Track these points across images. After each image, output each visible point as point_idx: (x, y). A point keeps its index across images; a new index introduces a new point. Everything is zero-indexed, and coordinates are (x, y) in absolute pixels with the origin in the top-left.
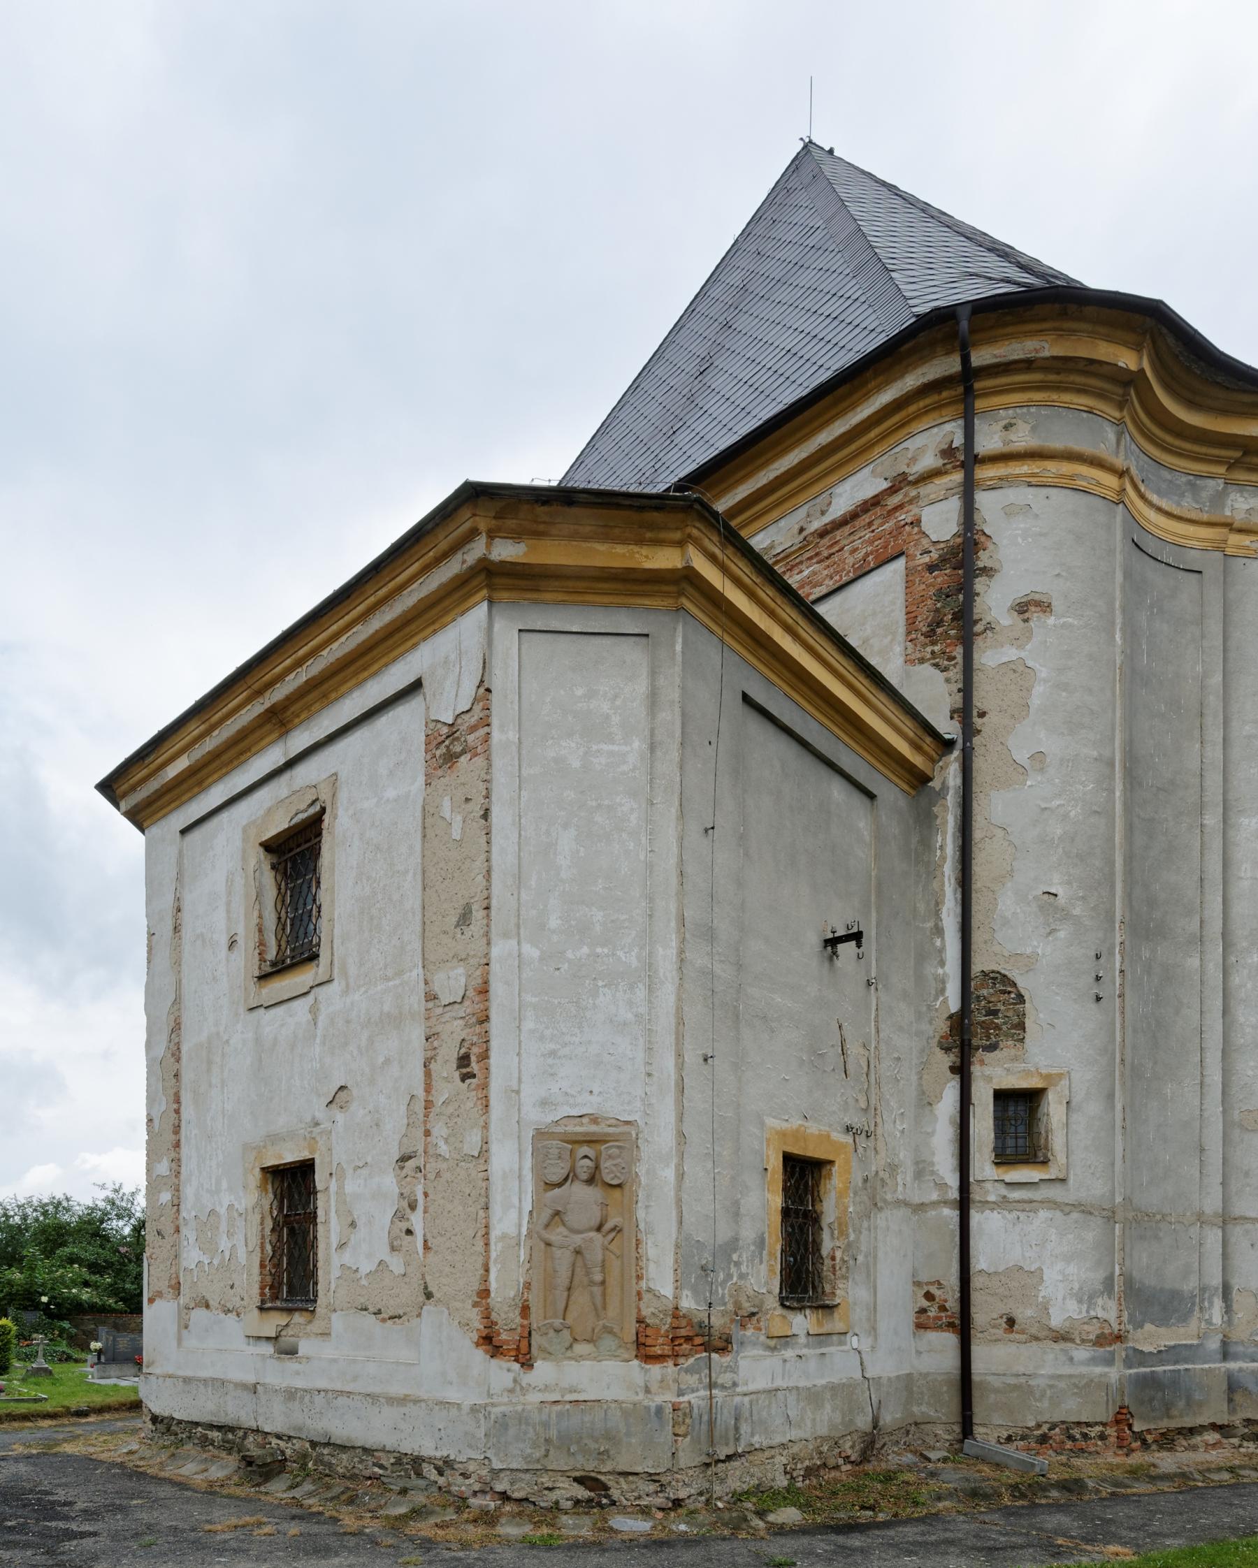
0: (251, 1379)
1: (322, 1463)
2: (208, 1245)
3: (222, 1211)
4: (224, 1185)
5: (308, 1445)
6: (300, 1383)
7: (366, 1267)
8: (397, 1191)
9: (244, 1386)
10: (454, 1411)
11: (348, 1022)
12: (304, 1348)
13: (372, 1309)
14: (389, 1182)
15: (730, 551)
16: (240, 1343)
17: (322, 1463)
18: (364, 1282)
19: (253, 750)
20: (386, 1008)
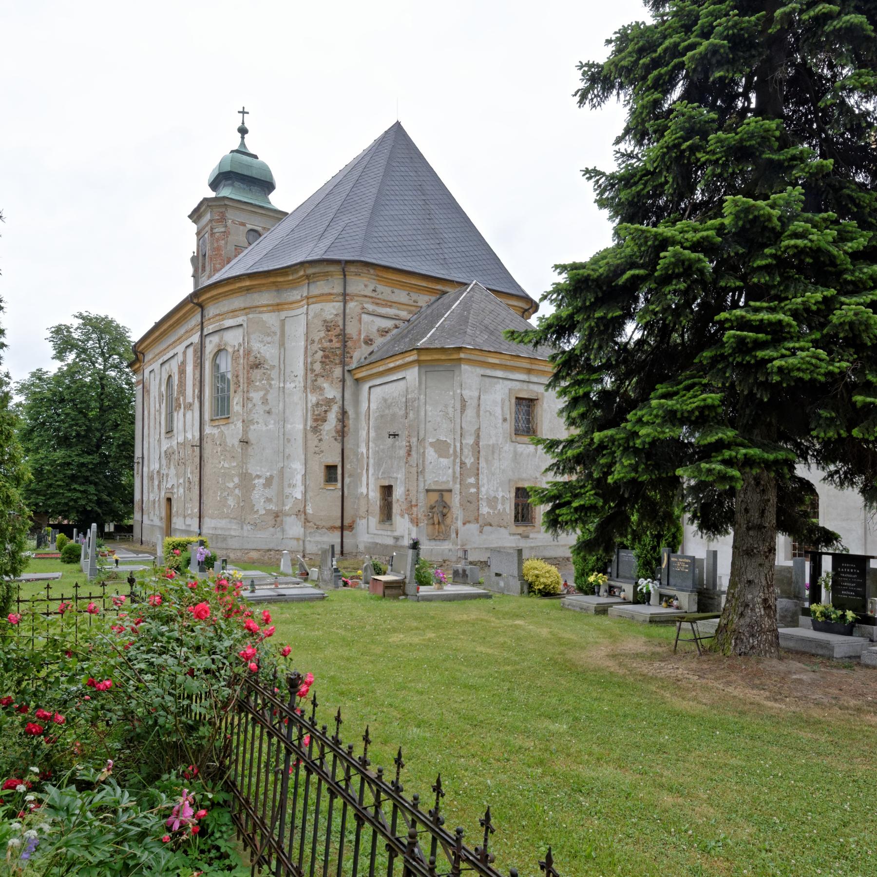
3: (500, 497)
4: (500, 489)
6: (532, 545)
12: (531, 536)
15: (450, 354)
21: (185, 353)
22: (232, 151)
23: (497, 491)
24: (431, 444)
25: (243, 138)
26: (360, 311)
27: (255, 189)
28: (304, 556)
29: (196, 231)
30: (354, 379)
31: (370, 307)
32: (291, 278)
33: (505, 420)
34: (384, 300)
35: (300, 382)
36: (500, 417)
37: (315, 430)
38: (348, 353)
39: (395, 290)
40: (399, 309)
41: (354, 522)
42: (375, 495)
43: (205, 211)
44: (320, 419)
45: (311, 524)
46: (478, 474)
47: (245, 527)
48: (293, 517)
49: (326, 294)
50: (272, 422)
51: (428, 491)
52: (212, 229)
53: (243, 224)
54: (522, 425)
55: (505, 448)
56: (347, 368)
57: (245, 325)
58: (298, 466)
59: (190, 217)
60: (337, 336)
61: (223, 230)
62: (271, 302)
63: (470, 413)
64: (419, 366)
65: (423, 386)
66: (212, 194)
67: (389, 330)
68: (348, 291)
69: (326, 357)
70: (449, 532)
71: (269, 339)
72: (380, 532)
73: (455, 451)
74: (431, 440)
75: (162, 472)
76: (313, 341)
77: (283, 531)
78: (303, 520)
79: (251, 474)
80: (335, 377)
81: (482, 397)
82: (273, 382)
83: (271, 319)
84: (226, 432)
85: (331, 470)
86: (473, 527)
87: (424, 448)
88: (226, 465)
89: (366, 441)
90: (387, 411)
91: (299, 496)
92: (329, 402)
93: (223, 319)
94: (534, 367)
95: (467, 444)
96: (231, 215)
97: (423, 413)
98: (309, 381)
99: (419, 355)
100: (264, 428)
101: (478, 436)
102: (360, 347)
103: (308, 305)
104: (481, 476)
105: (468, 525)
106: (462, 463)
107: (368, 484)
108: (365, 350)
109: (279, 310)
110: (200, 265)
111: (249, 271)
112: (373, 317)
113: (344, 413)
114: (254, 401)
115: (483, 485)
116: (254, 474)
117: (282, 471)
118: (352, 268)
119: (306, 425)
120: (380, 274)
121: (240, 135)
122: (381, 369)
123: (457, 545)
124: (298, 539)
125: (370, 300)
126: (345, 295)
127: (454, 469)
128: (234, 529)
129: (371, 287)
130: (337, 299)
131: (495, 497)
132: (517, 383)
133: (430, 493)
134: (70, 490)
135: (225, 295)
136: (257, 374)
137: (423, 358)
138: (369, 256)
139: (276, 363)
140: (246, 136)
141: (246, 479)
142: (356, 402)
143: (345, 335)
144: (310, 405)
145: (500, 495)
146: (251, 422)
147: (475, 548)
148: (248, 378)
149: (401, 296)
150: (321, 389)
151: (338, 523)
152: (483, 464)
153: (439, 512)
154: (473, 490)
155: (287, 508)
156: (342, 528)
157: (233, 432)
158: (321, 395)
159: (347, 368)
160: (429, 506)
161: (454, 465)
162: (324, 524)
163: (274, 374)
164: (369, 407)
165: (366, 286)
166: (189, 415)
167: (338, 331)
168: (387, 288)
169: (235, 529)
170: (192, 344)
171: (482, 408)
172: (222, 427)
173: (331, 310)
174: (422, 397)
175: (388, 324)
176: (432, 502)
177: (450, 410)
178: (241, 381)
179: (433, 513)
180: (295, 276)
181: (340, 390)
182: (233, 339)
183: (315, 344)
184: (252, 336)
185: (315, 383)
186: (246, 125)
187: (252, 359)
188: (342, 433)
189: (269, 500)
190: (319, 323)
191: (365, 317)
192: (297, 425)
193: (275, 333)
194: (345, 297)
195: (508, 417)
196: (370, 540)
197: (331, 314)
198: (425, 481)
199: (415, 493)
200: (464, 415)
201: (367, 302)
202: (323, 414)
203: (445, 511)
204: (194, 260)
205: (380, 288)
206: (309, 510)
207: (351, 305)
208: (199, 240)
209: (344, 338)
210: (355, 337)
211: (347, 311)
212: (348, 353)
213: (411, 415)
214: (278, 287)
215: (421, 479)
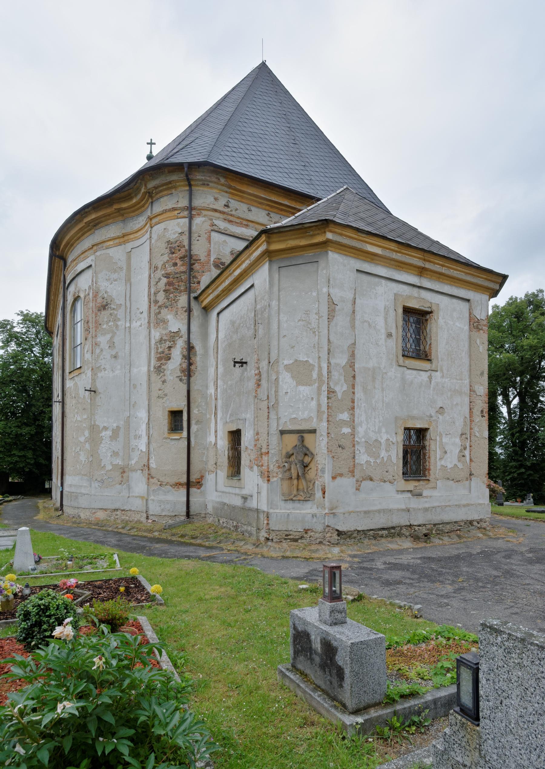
0: (403, 507)
1: (439, 530)
3: (383, 441)
4: (384, 430)
5: (432, 526)
6: (427, 505)
7: (450, 466)
8: (460, 444)
9: (403, 510)
10: (483, 506)
11: (443, 387)
12: (425, 493)
13: (451, 479)
14: (458, 440)
17: (439, 530)
18: (449, 470)
19: (404, 269)
20: (457, 388)
23: (380, 432)
24: (287, 368)
26: (210, 228)
28: (147, 518)
31: (222, 225)
32: (134, 201)
33: (389, 335)
34: (239, 218)
36: (383, 331)
37: (159, 370)
38: (194, 277)
39: (253, 208)
41: (202, 477)
42: (223, 443)
44: (165, 357)
45: (154, 481)
46: (353, 408)
47: (93, 485)
48: (139, 472)
50: (119, 367)
51: (282, 432)
54: (411, 345)
55: (389, 374)
58: (143, 414)
63: (341, 321)
64: (270, 261)
65: (276, 289)
69: (169, 284)
71: (115, 276)
73: (320, 374)
74: (286, 362)
76: (156, 268)
77: (129, 488)
78: (147, 475)
79: (98, 426)
80: (180, 306)
81: (358, 301)
82: (119, 323)
83: (117, 253)
85: (175, 415)
86: (347, 482)
87: (278, 373)
88: (79, 419)
90: (235, 337)
92: (174, 336)
94: (428, 265)
95: (337, 365)
98: (152, 315)
101: (353, 355)
103: (152, 227)
104: (357, 411)
105: (339, 479)
106: (331, 392)
107: (216, 432)
109: (125, 242)
112: (220, 229)
113: (190, 348)
114: (102, 346)
115: (360, 424)
117: (128, 421)
118: (198, 176)
119: (149, 366)
120: (233, 184)
122: (227, 282)
123: (324, 507)
124: (142, 498)
125: (221, 216)
126: (190, 208)
127: (318, 400)
130: (182, 214)
131: (376, 440)
133: (286, 436)
134: (10, 456)
136: (105, 314)
142: (205, 336)
143: (191, 257)
144: (153, 342)
145: (384, 437)
147: (350, 513)
150: (165, 322)
152: (359, 394)
153: (298, 464)
154: (346, 430)
155: (133, 462)
156: (188, 485)
158: (165, 329)
160: (284, 452)
161: (319, 394)
163: (120, 313)
164: (217, 337)
165: (216, 199)
167: (183, 252)
168: (242, 204)
171: (358, 316)
173: (174, 228)
174: (274, 303)
176: (289, 449)
177: (313, 317)
179: (291, 463)
181: (186, 321)
183: (159, 271)
184: (100, 276)
185: (159, 316)
187: (99, 300)
188: (188, 372)
189: (115, 454)
190: (162, 245)
191: (214, 235)
192: (142, 368)
193: (121, 268)
194: (191, 211)
195: (394, 331)
196: (218, 500)
197: (174, 234)
198: (278, 419)
199: (265, 435)
200: (332, 324)
202: (167, 351)
203: (307, 460)
205: (234, 204)
206: (153, 465)
207: (198, 221)
209: (190, 260)
210: (203, 258)
211: (194, 228)
212: (195, 277)
215: (273, 416)
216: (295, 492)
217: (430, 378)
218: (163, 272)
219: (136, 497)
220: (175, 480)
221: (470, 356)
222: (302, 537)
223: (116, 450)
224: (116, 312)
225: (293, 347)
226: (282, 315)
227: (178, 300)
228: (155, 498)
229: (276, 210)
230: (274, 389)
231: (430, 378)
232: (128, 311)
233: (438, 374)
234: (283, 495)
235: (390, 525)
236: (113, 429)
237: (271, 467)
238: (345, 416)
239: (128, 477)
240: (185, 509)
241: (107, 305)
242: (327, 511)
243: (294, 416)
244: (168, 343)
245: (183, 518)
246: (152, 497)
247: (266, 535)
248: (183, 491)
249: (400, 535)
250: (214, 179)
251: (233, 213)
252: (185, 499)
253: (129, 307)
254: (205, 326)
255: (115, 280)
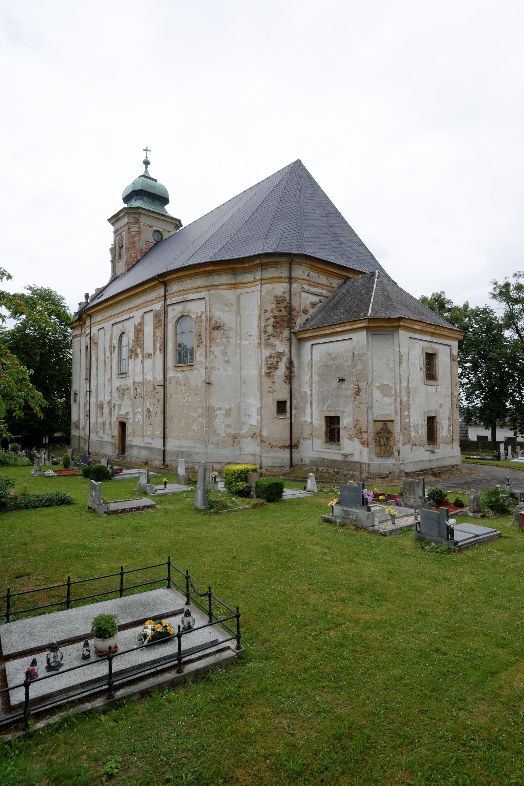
0: (428, 459)
2: (417, 432)
3: (420, 424)
6: (437, 458)
7: (445, 436)
9: (428, 460)
12: (436, 451)
14: (447, 422)
15: (392, 322)
16: (424, 452)
21: (142, 317)
22: (141, 176)
23: (418, 420)
24: (377, 387)
25: (146, 167)
26: (301, 290)
27: (157, 202)
29: (113, 230)
30: (298, 338)
31: (306, 287)
32: (247, 265)
34: (315, 282)
35: (255, 340)
37: (269, 375)
39: (320, 276)
40: (322, 289)
41: (298, 442)
42: (320, 424)
43: (123, 217)
44: (272, 368)
47: (209, 446)
49: (277, 278)
50: (231, 369)
51: (375, 421)
52: (129, 229)
53: (151, 227)
56: (293, 331)
57: (207, 298)
59: (109, 220)
60: (285, 307)
61: (137, 230)
62: (229, 282)
64: (367, 331)
65: (370, 345)
66: (126, 205)
67: (317, 303)
68: (292, 276)
69: (276, 322)
70: (393, 451)
71: (227, 309)
72: (326, 450)
73: (396, 392)
74: (377, 384)
75: (113, 402)
76: (266, 311)
77: (240, 448)
79: (214, 407)
82: (231, 340)
83: (229, 294)
84: (190, 376)
85: (281, 406)
86: (408, 447)
87: (372, 390)
88: (190, 400)
89: (308, 382)
90: (331, 362)
91: (255, 423)
92: (280, 355)
93: (187, 294)
94: (437, 332)
95: (403, 387)
96: (144, 220)
97: (370, 365)
99: (368, 323)
100: (224, 373)
102: (301, 316)
103: (262, 285)
105: (405, 446)
106: (401, 401)
108: (304, 318)
109: (235, 288)
110: (117, 254)
111: (213, 260)
112: (309, 294)
114: (216, 353)
116: (216, 407)
117: (239, 405)
120: (313, 264)
121: (144, 166)
124: (254, 455)
127: (395, 405)
128: (199, 448)
129: (307, 274)
130: (285, 281)
132: (426, 343)
133: (377, 423)
135: (189, 276)
136: (218, 334)
137: (371, 325)
138: (307, 251)
139: (233, 326)
140: (148, 166)
141: (209, 412)
142: (299, 355)
144: (264, 357)
146: (213, 368)
147: (410, 462)
148: (210, 337)
149: (323, 280)
150: (273, 345)
151: (288, 443)
152: (411, 402)
153: (383, 437)
154: (407, 420)
157: (196, 376)
158: (274, 350)
159: (293, 331)
160: (376, 432)
161: (395, 402)
162: (277, 444)
163: (232, 334)
164: (312, 358)
165: (303, 272)
166: (148, 363)
168: (315, 274)
169: (199, 448)
170: (152, 310)
172: (187, 373)
174: (369, 353)
175: (316, 299)
177: (391, 363)
178: (204, 338)
180: (251, 264)
181: (288, 346)
182: (195, 309)
183: (268, 313)
186: (149, 159)
187: (213, 323)
188: (289, 378)
191: (303, 293)
193: (232, 305)
194: (291, 279)
196: (315, 456)
198: (373, 414)
201: (305, 284)
202: (275, 364)
203: (388, 435)
204: (113, 250)
205: (312, 274)
206: (265, 434)
207: (294, 285)
208: (116, 237)
209: (290, 308)
210: (298, 309)
213: (359, 366)
214: (235, 272)
215: (370, 412)
216: (383, 453)
217: (436, 389)
218: (272, 314)
219: (247, 455)
220: (282, 444)
221: (451, 375)
222: (388, 476)
223: (228, 424)
224: (228, 333)
225: (380, 377)
226: (374, 360)
227: (283, 333)
228: (268, 455)
229: (330, 276)
230: (370, 398)
231: (436, 389)
232: (239, 333)
233: (439, 387)
234: (376, 454)
235: (424, 468)
236: (226, 410)
237: (369, 439)
238: (406, 413)
239: (240, 441)
240: (289, 462)
241: (220, 327)
242: (401, 462)
243: (382, 413)
244: (276, 359)
245: (288, 468)
246: (264, 455)
247: (367, 476)
248: (288, 451)
249: (427, 474)
250: (305, 262)
251: (311, 280)
252: (289, 456)
253: (239, 331)
254: (299, 349)
255: (227, 312)
